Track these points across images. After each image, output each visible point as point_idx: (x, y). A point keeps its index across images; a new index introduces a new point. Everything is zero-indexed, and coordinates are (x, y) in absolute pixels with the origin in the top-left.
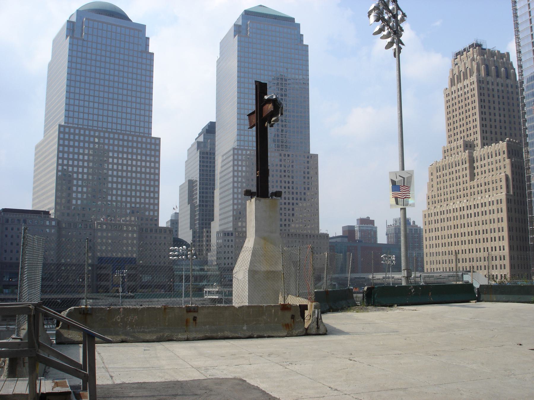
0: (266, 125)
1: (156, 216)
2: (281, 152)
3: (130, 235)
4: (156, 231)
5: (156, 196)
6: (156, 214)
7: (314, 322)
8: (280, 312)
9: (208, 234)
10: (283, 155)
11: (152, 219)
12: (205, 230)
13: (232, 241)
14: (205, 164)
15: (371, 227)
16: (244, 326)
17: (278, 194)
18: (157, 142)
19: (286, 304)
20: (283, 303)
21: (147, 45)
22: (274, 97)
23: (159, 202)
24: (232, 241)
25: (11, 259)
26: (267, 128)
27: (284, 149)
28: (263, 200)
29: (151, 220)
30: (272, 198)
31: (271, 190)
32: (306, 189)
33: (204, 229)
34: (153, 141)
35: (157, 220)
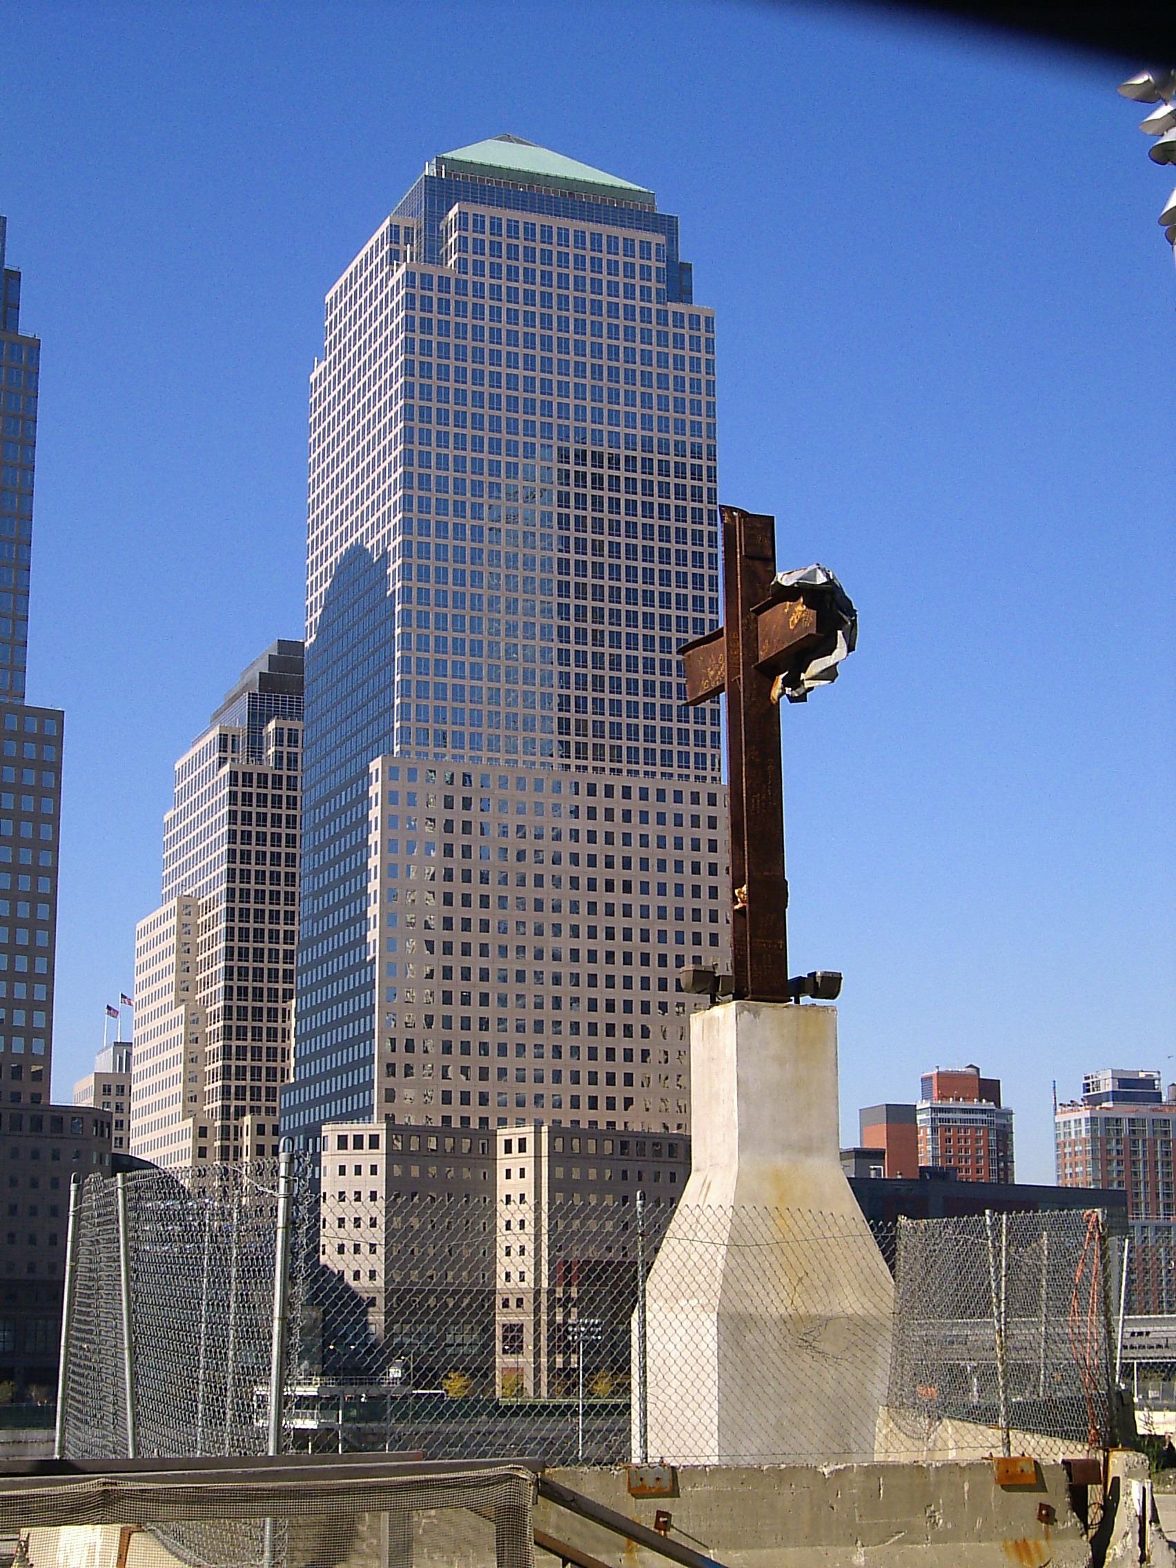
0: (775, 692)
1: (36, 1059)
2: (591, 777)
3: (592, 1174)
4: (37, 1124)
5: (41, 967)
6: (38, 1047)
7: (1127, 1533)
8: (994, 1491)
9: (203, 1142)
10: (600, 791)
11: (20, 1067)
12: (247, 1120)
13: (374, 1170)
14: (28, 803)
15: (983, 1111)
16: (852, 1553)
17: (828, 986)
18: (50, 727)
19: (1015, 1460)
20: (1001, 1455)
21: (12, 307)
22: (821, 579)
23: (50, 995)
24: (374, 1170)
25: (31, 1268)
26: (773, 711)
27: (675, 770)
28: (768, 1011)
29: (17, 1073)
30: (797, 1001)
31: (796, 969)
32: (705, 939)
33: (244, 1115)
34: (33, 726)
35: (43, 1077)
